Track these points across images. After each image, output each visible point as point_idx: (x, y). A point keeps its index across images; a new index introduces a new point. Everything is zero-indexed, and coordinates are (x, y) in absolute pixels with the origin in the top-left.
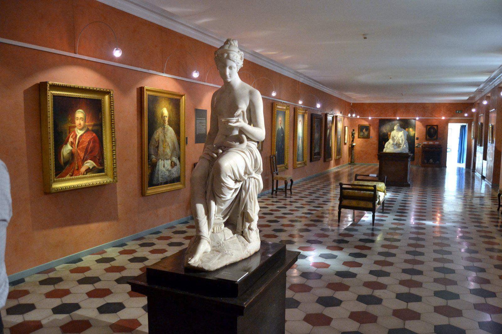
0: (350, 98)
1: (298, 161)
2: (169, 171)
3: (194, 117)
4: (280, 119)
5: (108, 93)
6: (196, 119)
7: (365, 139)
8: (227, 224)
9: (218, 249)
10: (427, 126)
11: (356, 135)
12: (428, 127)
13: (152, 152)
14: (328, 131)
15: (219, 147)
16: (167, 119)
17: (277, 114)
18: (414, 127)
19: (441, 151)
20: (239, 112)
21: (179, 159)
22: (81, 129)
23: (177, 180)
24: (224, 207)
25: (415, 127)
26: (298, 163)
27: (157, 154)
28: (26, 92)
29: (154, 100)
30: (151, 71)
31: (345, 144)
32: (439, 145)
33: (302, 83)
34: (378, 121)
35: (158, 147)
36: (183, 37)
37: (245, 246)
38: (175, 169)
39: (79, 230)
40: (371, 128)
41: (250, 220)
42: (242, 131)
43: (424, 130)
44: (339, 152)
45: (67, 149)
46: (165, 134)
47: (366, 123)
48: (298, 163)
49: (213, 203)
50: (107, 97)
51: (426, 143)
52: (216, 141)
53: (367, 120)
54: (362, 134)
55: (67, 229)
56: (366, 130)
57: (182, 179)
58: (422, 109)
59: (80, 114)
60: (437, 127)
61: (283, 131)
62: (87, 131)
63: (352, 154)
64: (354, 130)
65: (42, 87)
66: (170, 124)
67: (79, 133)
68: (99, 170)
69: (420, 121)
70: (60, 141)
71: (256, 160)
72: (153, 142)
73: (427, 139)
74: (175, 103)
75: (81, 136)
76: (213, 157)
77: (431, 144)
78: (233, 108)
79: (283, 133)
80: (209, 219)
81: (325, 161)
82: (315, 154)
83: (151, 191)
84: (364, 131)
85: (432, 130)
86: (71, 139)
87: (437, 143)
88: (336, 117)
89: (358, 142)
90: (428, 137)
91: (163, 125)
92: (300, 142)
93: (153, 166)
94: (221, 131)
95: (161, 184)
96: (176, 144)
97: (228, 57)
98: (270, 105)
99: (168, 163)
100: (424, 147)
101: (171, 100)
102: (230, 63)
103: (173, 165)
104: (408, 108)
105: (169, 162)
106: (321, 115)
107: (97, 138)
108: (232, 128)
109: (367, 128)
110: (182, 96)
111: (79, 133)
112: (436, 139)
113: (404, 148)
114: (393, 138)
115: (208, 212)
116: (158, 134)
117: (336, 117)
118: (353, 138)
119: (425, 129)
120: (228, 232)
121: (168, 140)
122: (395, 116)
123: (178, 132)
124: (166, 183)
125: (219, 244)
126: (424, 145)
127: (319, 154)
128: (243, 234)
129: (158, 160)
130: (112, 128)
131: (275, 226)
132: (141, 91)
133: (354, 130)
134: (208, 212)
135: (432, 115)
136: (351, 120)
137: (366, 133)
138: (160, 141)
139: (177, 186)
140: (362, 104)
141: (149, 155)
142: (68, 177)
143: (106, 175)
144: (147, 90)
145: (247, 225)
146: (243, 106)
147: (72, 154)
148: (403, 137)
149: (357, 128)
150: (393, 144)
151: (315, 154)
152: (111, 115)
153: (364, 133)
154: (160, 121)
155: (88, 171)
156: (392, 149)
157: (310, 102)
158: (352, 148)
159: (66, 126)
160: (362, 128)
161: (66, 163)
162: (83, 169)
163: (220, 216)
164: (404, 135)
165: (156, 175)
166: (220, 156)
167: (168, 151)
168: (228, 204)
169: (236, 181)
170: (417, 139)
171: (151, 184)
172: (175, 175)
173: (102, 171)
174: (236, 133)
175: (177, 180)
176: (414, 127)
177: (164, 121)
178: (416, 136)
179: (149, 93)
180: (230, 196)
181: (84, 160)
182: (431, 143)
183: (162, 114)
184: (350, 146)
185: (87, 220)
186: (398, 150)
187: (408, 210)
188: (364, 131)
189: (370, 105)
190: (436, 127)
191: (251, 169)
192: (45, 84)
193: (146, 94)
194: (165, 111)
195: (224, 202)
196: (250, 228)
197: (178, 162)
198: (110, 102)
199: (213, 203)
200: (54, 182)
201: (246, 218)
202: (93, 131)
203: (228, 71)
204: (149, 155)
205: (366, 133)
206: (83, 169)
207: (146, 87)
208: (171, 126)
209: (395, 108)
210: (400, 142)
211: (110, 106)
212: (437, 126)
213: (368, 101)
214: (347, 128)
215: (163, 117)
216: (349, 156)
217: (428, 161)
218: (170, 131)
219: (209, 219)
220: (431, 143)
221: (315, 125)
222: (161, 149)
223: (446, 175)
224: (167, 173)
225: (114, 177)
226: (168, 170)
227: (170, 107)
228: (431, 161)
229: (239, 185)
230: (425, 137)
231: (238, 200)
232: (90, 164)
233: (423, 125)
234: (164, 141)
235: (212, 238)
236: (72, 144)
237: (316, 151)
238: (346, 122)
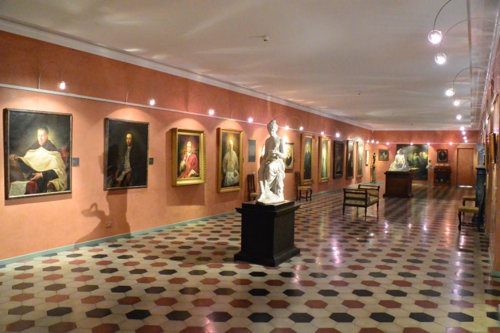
0: (371, 127)
1: (322, 177)
2: (233, 179)
3: (248, 145)
4: (308, 145)
5: (203, 132)
6: (249, 147)
7: (385, 162)
8: (271, 190)
9: (267, 198)
10: (438, 150)
11: (377, 158)
12: (439, 151)
13: (224, 167)
14: (349, 155)
15: (268, 161)
16: (232, 146)
17: (305, 143)
18: (427, 151)
19: (450, 172)
20: (276, 148)
21: (239, 171)
22: (190, 153)
23: (237, 185)
24: (270, 183)
25: (428, 151)
26: (322, 179)
27: (226, 168)
28: (167, 133)
29: (225, 135)
30: (224, 118)
31: (367, 165)
32: (449, 167)
33: (326, 118)
34: (396, 146)
35: (227, 164)
36: (242, 95)
37: (278, 198)
38: (236, 177)
39: (187, 208)
40: (390, 152)
41: (280, 188)
42: (277, 155)
43: (436, 154)
44: (360, 172)
45: (183, 163)
46: (231, 155)
47: (385, 148)
48: (322, 179)
49: (266, 181)
50: (202, 134)
51: (437, 165)
52: (267, 159)
53: (385, 145)
54: (382, 157)
55: (181, 207)
56: (385, 154)
57: (240, 184)
58: (434, 136)
59: (189, 144)
60: (447, 152)
61: (310, 155)
62: (192, 153)
63: (373, 174)
64: (375, 154)
65: (174, 131)
66: (234, 150)
67: (189, 154)
68: (197, 176)
69: (433, 146)
70: (180, 159)
71: (282, 166)
72: (224, 161)
73: (438, 162)
74: (237, 137)
75: (190, 156)
76: (266, 164)
77: (442, 166)
78: (274, 146)
79: (310, 156)
80: (264, 186)
81: (347, 179)
82: (337, 173)
83: (223, 190)
84: (384, 154)
85: (443, 154)
86: (185, 158)
87: (447, 165)
88: (357, 142)
89: (379, 164)
90: (439, 160)
91: (230, 151)
92: (324, 163)
93: (224, 175)
94: (269, 155)
95: (228, 186)
96: (237, 162)
97: (272, 128)
98: (299, 135)
99: (232, 174)
100: (436, 169)
101: (235, 134)
102: (273, 129)
103: (235, 175)
104: (421, 134)
105: (233, 173)
106: (342, 142)
107: (196, 158)
108: (274, 154)
109: (387, 152)
110: (241, 132)
111: (189, 154)
112: (447, 162)
113: (404, 168)
114: (397, 160)
115: (264, 184)
116: (227, 156)
117: (357, 142)
118: (374, 160)
119: (436, 153)
120: (271, 193)
121: (233, 159)
122: (410, 141)
123: (238, 155)
124: (231, 186)
125: (268, 196)
126: (436, 166)
127: (341, 172)
128: (277, 194)
129: (227, 171)
130: (205, 152)
131: (306, 224)
132: (218, 130)
133: (375, 154)
134: (264, 184)
135: (442, 141)
136: (373, 147)
137: (385, 156)
138: (228, 160)
139: (237, 188)
140: (382, 131)
141: (222, 168)
142: (183, 178)
143: (200, 179)
144: (222, 130)
145: (279, 190)
146: (278, 145)
147: (185, 166)
148: (404, 159)
149: (378, 152)
150: (396, 165)
151: (337, 173)
152: (204, 145)
153: (383, 156)
154: (228, 148)
155: (192, 175)
156: (396, 168)
157: (331, 133)
158: (373, 169)
159: (183, 151)
160: (381, 152)
161: (182, 171)
162: (190, 175)
163: (269, 187)
164: (405, 158)
165: (225, 181)
166: (269, 164)
167: (233, 166)
168: (272, 181)
169: (275, 173)
170: (430, 161)
171: (223, 186)
172: (236, 181)
173: (198, 176)
174: (275, 155)
175: (237, 185)
176: (427, 151)
177: (231, 147)
178: (429, 159)
179: (222, 131)
180: (272, 178)
181: (190, 169)
182: (442, 165)
183: (230, 143)
184: (372, 167)
185: (190, 203)
186: (400, 169)
187: (432, 223)
188: (384, 154)
189: (389, 132)
190: (446, 151)
191: (280, 169)
192: (176, 129)
193: (221, 131)
194: (231, 141)
195: (270, 181)
196: (280, 192)
197: (238, 173)
198: (204, 137)
199: (266, 181)
200: (178, 180)
201: (278, 187)
202: (195, 154)
203: (272, 132)
204: (222, 168)
205: (385, 156)
206: (190, 175)
207: (222, 128)
208: (234, 151)
209: (410, 135)
210: (402, 163)
211: (204, 139)
212: (447, 150)
213: (387, 129)
214: (368, 152)
215: (230, 145)
216: (371, 176)
217: (439, 180)
218: (234, 154)
219: (264, 186)
220: (442, 165)
221: (337, 150)
222: (228, 165)
223: (47, 111)
224: (232, 180)
225: (205, 180)
226: (232, 178)
227: (234, 139)
228: (442, 180)
229: (276, 175)
230: (436, 160)
231: (275, 181)
232: (193, 172)
233: (435, 149)
234: (230, 160)
235: (266, 194)
236: (185, 160)
237: (338, 171)
238: (368, 147)
